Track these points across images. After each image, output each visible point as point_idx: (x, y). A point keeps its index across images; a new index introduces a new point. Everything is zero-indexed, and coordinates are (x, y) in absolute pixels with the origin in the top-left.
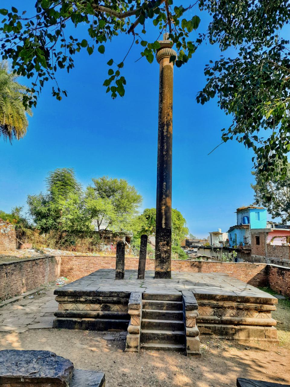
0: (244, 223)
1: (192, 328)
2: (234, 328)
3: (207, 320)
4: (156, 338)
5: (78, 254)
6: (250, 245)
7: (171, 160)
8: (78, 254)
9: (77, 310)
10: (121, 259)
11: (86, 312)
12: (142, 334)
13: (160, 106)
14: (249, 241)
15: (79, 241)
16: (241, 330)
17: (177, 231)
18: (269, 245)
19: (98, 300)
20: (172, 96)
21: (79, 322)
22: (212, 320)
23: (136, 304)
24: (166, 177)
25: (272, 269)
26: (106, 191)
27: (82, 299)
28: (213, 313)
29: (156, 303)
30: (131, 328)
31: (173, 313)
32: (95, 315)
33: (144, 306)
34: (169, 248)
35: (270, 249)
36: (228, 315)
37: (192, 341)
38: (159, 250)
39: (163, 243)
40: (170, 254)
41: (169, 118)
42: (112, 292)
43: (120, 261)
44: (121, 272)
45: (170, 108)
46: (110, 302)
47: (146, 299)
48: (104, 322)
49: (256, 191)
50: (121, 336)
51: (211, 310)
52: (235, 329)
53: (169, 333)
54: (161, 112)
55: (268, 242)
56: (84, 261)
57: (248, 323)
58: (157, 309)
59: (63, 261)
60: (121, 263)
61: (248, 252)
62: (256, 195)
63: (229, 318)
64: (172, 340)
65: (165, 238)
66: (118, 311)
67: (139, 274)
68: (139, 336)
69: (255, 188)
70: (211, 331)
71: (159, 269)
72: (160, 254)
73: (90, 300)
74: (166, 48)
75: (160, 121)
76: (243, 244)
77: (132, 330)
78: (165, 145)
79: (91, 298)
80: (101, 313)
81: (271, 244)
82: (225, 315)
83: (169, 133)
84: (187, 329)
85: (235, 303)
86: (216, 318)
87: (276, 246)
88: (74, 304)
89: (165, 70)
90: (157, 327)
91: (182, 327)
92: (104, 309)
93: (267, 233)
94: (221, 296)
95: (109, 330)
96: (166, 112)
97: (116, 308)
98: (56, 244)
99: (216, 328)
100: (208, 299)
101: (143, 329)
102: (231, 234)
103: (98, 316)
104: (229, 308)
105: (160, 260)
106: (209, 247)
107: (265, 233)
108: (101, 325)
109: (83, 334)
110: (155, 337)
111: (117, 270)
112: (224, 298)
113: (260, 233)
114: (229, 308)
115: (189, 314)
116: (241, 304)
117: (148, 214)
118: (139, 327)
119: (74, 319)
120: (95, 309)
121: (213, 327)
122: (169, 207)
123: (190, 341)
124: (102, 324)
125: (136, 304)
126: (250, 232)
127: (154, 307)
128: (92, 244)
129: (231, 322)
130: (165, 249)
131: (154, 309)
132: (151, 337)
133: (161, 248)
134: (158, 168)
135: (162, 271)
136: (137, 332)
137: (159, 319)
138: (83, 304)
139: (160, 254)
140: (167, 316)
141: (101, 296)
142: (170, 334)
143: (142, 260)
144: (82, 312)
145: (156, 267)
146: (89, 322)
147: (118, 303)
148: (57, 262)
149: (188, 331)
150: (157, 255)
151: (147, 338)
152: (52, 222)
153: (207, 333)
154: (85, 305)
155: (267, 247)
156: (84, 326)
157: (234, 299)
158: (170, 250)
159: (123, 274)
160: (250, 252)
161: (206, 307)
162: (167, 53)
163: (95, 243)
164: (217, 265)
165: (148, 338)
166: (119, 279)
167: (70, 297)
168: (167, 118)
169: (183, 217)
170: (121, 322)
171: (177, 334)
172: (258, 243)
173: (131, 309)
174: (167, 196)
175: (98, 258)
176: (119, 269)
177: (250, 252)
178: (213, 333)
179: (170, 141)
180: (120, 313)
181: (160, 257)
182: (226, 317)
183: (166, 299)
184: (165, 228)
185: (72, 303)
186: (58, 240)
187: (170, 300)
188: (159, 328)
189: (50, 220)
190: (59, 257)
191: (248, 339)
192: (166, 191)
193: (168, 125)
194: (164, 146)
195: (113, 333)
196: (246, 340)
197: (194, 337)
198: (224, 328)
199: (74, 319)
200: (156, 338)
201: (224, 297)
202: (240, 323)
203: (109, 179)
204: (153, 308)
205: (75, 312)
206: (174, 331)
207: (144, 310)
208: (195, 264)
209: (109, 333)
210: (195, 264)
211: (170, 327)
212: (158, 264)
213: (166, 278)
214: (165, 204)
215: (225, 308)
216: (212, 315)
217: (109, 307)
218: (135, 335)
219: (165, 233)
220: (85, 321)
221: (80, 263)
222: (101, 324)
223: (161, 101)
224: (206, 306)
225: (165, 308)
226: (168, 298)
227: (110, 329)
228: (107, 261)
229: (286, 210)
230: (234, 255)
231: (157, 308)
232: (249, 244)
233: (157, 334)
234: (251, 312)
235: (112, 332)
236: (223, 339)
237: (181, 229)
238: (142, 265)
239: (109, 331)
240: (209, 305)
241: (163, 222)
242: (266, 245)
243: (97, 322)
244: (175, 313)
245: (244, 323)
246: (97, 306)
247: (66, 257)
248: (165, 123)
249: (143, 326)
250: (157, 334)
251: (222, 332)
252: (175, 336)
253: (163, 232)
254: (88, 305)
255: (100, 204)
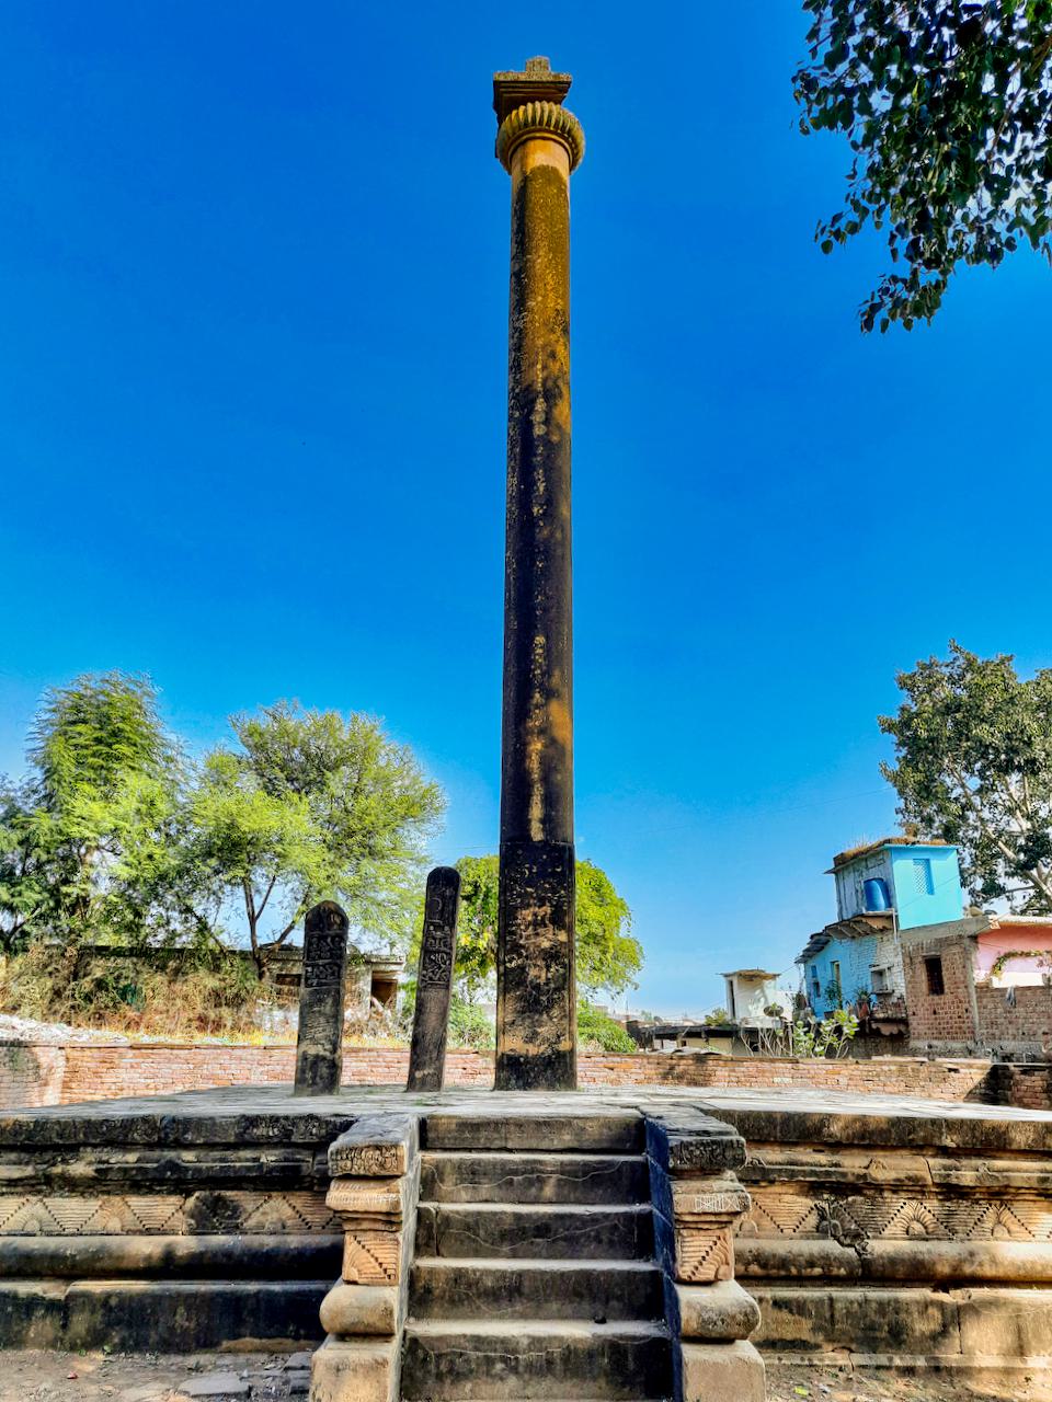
0: (871, 904)
1: (715, 1295)
2: (932, 1303)
3: (784, 1263)
4: (499, 1366)
5: (143, 1037)
6: (901, 998)
7: (564, 543)
8: (143, 1037)
9: (49, 1234)
10: (329, 993)
11: (96, 1241)
12: (412, 1346)
13: (517, 325)
14: (898, 982)
15: (154, 982)
16: (973, 1309)
17: (595, 951)
18: (984, 989)
19: (173, 1166)
20: (565, 284)
21: (53, 1306)
22: (811, 1264)
23: (378, 1147)
24: (546, 610)
25: (1017, 1084)
26: (296, 771)
27: (80, 1168)
28: (813, 1220)
29: (494, 1164)
30: (346, 1302)
31: (594, 1219)
32: (149, 1257)
33: (429, 1184)
34: (563, 937)
35: (991, 1006)
36: (895, 1228)
37: (717, 1370)
38: (516, 949)
39: (535, 915)
40: (569, 968)
41: (555, 367)
42: (252, 1121)
43: (320, 1001)
44: (324, 1058)
45: (558, 330)
46: (238, 1181)
47: (445, 1150)
48: (194, 1296)
49: (901, 793)
50: (291, 1374)
51: (803, 1204)
52: (941, 1306)
53: (579, 1331)
54: (518, 347)
55: (980, 975)
56: (174, 1066)
57: (1011, 1273)
58: (502, 1201)
59: (73, 1072)
60: (328, 1008)
61: (894, 1029)
62: (903, 806)
63: (906, 1247)
64: (594, 1379)
65: (546, 891)
66: (283, 1229)
67: (415, 1064)
68: (391, 1351)
69: (897, 780)
70: (807, 1324)
71: (515, 1044)
72: (522, 968)
73: (125, 1170)
74: (538, 104)
75: (517, 382)
76: (873, 997)
77: (347, 1321)
78: (540, 474)
79: (132, 1157)
80: (186, 1244)
81: (996, 983)
82: (879, 1231)
83: (559, 427)
84: (685, 1294)
85: (932, 1161)
86: (831, 1246)
87: (1017, 989)
88: (33, 1199)
89: (537, 184)
90: (505, 1303)
91: (654, 1297)
92: (202, 1223)
93: (974, 938)
94: (856, 1119)
95: (225, 1344)
96: (540, 342)
97: (274, 1216)
98: (52, 1001)
99: (838, 1306)
100: (784, 1143)
101: (418, 1317)
102: (814, 968)
103: (167, 1267)
104: (897, 1187)
105: (520, 998)
106: (728, 1029)
107: (967, 942)
108: (181, 1319)
109: (62, 1372)
110: (489, 1361)
111: (303, 1047)
112: (872, 1133)
113: (943, 943)
114: (897, 1187)
115: (696, 1197)
116: (965, 1162)
117: (470, 879)
118: (394, 1296)
119: (24, 1288)
120: (154, 1225)
121: (821, 1301)
122: (563, 748)
123: (704, 1367)
124: (188, 1309)
125: (378, 1147)
126: (897, 942)
127: (485, 1189)
128: (217, 998)
129: (917, 1273)
130: (546, 944)
131: (486, 1201)
132: (468, 1361)
133: (527, 938)
134: (507, 576)
135: (532, 1050)
136: (381, 1325)
137: (514, 1255)
138: (82, 1194)
139: (522, 968)
140: (562, 1233)
141: (190, 1146)
142: (581, 1340)
143: (433, 995)
144: (70, 1246)
145: (502, 1030)
146: (113, 1302)
147: (284, 1181)
148: (42, 1072)
149: (690, 1305)
150: (505, 974)
151: (444, 1367)
152: (39, 897)
153: (789, 1337)
154: (93, 1204)
155: (979, 999)
156: (80, 1323)
157: (925, 1138)
158: (570, 944)
159: (335, 1067)
160: (903, 1028)
161: (776, 1189)
162: (542, 116)
163: (230, 993)
164: (775, 1073)
165: (451, 1371)
166: (313, 1094)
167: (13, 1156)
168: (544, 368)
169: (617, 894)
170: (299, 1293)
171: (622, 1337)
172: (936, 986)
173: (347, 1177)
174: (549, 694)
175: (238, 1052)
176: (315, 1042)
177: (903, 1028)
178: (820, 1338)
179: (559, 462)
180: (294, 1241)
181: (521, 983)
182: (886, 1245)
183: (556, 1144)
184: (545, 843)
185: (20, 1194)
186: (62, 984)
187: (575, 1145)
188: (519, 1307)
189: (29, 887)
190: (54, 1052)
191: (1018, 1363)
192: (548, 673)
193: (551, 396)
194: (534, 483)
195: (249, 1365)
196: (1008, 1372)
197: (727, 1341)
198: (882, 1306)
199: (24, 1288)
200: (499, 1366)
201: (872, 1127)
202: (968, 1269)
203: (301, 721)
204: (484, 1194)
205: (35, 1244)
206: (602, 1321)
207: (430, 1205)
208: (678, 1070)
209: (228, 1360)
210: (678, 1070)
211: (580, 1295)
212: (509, 1019)
213: (551, 1087)
214: (542, 731)
215: (879, 1188)
216: (807, 1236)
217: (236, 1211)
218: (365, 1345)
219: (543, 865)
220: (86, 1295)
221: (155, 1076)
222: (181, 1310)
223: (520, 303)
224: (772, 1182)
225: (549, 1191)
226: (567, 1139)
227: (237, 1336)
228: (279, 1068)
229: (1022, 869)
230: (845, 1030)
231: (502, 1193)
232: (897, 994)
233: (504, 1343)
234: (1020, 1208)
235: (242, 1358)
236: (878, 1368)
237: (611, 944)
238: (432, 1020)
239: (229, 1351)
240: (790, 1176)
241: (536, 811)
242: (972, 990)
243: (157, 1299)
244: (606, 1216)
245: (989, 1271)
246: (163, 1206)
247: (88, 1052)
248: (539, 387)
249: (421, 1297)
250: (504, 1341)
251: (872, 1327)
252: (615, 1347)
253: (533, 863)
254: (116, 1200)
255: (260, 814)
